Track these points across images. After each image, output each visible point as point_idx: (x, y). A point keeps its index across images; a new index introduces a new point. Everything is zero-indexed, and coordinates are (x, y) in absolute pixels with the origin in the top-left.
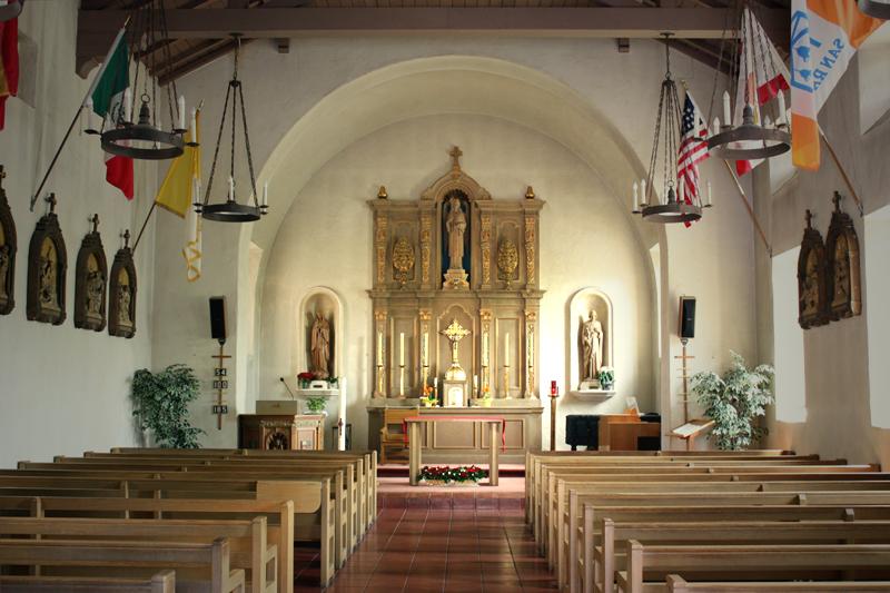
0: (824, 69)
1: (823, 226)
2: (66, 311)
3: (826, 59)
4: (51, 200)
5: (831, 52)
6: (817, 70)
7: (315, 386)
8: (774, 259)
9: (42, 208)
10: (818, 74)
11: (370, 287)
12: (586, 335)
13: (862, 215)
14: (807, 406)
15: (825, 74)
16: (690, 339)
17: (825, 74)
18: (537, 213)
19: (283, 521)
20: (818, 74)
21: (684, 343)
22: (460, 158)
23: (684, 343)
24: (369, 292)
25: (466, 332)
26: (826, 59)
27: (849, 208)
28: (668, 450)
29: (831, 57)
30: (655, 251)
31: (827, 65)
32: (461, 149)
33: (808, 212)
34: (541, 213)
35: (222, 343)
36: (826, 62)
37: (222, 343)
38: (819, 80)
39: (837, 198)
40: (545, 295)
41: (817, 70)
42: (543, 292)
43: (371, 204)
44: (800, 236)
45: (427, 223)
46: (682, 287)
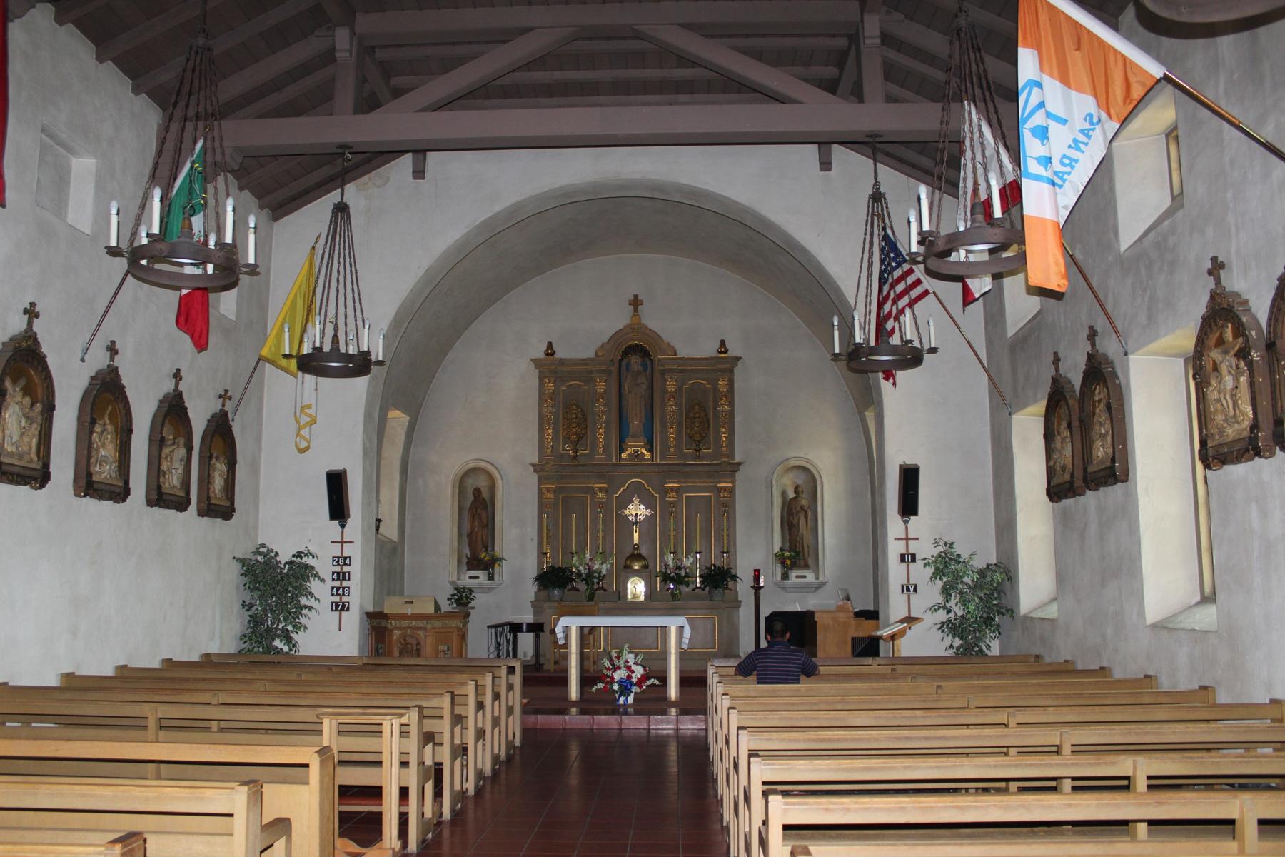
0: (1073, 154)
1: (1075, 373)
2: (191, 496)
3: (1075, 141)
4: (112, 349)
5: (1082, 131)
6: (1064, 156)
7: (798, 577)
8: (1014, 417)
9: (98, 359)
10: (1066, 161)
11: (535, 460)
12: (792, 515)
13: (1126, 354)
14: (124, 387)
15: (1076, 161)
16: (912, 518)
17: (1076, 161)
18: (731, 371)
19: (678, 672)
20: (1066, 161)
21: (906, 523)
22: (640, 307)
23: (906, 523)
24: (533, 465)
25: (648, 512)
26: (1075, 141)
27: (1109, 346)
28: (885, 656)
29: (1081, 138)
30: (870, 415)
31: (1078, 149)
32: (640, 298)
33: (1056, 354)
34: (736, 370)
35: (343, 526)
36: (1076, 145)
37: (343, 526)
38: (1068, 169)
39: (1092, 335)
40: (741, 467)
41: (1064, 156)
42: (739, 464)
43: (536, 362)
44: (1047, 388)
45: (601, 387)
46: (896, 455)
